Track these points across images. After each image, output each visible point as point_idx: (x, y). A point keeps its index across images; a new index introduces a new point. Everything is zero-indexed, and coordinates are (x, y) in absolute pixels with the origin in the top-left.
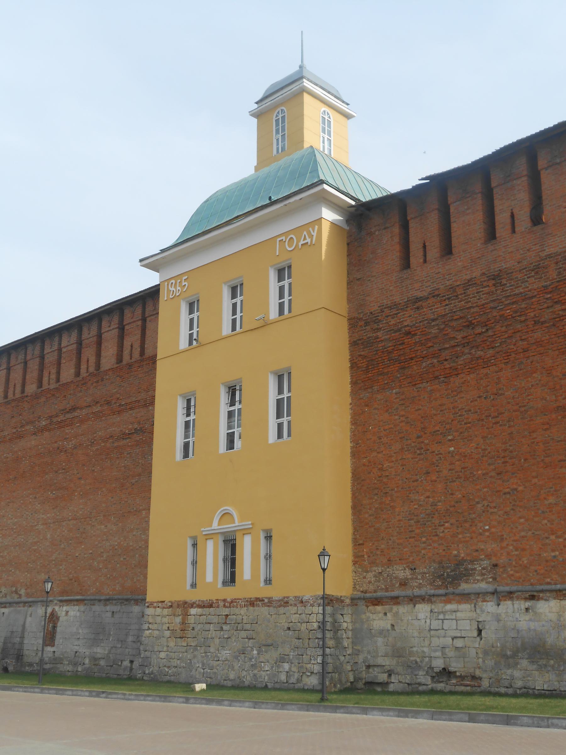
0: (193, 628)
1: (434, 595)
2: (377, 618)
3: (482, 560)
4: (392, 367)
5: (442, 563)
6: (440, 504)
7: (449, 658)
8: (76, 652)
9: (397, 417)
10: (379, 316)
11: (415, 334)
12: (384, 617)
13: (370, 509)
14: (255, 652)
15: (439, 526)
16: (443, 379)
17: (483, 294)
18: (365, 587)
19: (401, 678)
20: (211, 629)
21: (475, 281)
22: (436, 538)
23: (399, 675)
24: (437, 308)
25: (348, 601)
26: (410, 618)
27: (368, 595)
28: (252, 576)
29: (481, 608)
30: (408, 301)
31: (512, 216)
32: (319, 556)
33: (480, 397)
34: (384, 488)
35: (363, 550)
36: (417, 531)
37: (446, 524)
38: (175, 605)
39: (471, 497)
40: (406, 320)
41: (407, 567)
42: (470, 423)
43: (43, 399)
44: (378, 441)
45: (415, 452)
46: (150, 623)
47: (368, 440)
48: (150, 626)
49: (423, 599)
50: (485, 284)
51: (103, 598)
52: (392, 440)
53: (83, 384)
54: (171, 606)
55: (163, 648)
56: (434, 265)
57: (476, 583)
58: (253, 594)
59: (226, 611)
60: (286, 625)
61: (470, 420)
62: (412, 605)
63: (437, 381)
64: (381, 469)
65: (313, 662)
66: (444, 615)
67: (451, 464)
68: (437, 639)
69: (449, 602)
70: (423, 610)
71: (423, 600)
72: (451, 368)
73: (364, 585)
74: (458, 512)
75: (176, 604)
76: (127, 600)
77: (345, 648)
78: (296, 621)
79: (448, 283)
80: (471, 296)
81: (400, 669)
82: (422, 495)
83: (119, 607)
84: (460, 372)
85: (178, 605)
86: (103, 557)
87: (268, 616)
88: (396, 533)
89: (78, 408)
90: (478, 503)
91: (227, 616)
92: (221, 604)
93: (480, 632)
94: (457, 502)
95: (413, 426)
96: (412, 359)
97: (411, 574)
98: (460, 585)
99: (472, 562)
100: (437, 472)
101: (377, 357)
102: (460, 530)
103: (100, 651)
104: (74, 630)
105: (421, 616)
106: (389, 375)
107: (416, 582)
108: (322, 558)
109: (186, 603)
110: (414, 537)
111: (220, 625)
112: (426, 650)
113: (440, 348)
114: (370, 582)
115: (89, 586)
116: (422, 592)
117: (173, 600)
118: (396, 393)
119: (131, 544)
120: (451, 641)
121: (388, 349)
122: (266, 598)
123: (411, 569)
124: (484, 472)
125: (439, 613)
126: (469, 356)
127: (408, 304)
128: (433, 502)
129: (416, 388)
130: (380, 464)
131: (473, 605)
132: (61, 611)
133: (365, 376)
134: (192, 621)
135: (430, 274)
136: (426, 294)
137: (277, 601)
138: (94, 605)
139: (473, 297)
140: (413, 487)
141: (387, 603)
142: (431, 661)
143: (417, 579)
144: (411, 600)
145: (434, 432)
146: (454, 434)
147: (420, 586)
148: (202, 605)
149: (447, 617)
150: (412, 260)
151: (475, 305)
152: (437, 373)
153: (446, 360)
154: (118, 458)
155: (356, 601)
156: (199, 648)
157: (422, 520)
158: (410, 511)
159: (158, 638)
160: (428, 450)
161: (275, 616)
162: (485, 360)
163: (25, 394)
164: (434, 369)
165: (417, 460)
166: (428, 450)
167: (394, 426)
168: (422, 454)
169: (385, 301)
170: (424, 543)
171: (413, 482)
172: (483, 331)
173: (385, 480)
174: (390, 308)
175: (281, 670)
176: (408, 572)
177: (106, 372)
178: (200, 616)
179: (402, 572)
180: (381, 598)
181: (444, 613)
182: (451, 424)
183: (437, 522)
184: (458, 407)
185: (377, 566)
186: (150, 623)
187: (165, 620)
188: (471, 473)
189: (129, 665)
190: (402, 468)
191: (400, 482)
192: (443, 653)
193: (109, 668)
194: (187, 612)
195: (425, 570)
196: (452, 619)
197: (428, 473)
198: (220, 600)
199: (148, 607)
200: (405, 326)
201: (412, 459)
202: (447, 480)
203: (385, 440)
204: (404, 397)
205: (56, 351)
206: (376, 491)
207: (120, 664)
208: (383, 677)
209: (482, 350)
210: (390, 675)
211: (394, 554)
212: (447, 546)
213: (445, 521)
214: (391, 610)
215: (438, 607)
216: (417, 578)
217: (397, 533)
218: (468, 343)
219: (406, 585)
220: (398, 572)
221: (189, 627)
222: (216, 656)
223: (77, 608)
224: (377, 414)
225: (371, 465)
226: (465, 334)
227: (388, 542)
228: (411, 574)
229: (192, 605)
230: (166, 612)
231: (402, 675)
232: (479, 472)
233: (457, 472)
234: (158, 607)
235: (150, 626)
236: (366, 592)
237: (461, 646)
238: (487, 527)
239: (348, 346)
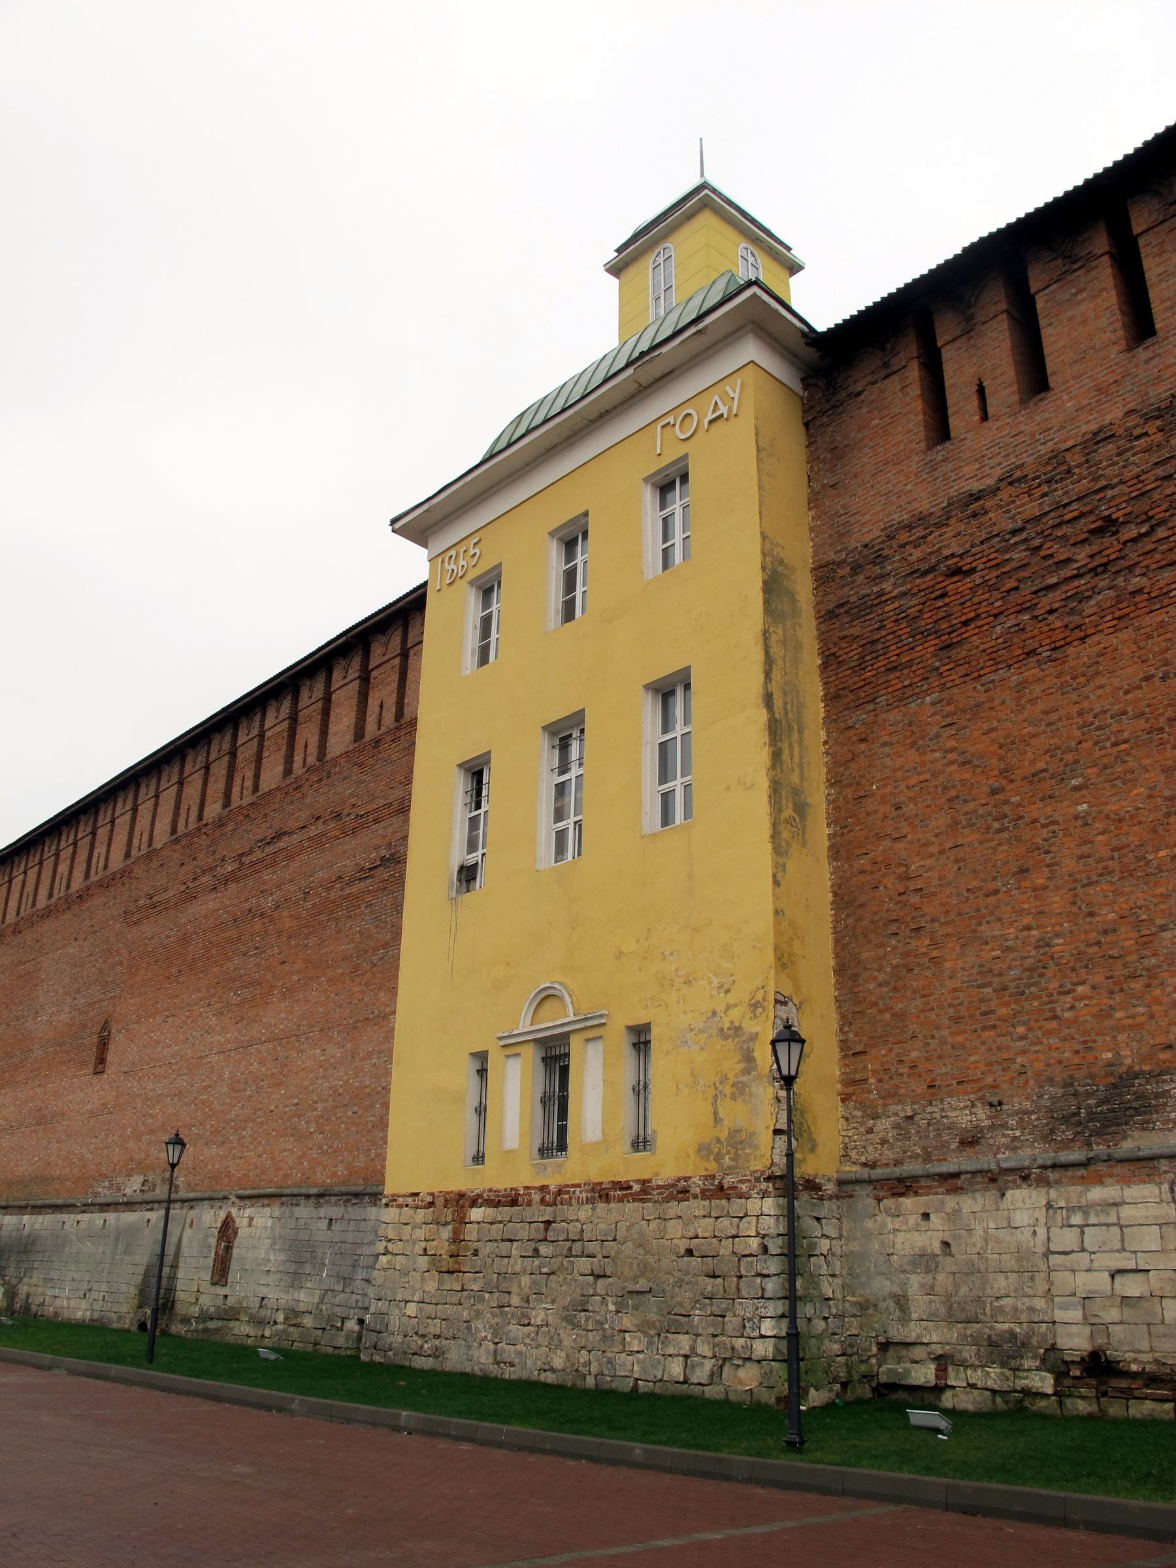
0: (476, 1250)
4: (921, 647)
5: (1071, 1084)
6: (1061, 941)
8: (263, 1298)
9: (937, 754)
11: (973, 570)
13: (879, 971)
15: (1060, 993)
16: (1048, 653)
17: (1134, 455)
18: (871, 1154)
19: (975, 1376)
20: (514, 1252)
21: (1110, 430)
23: (967, 1367)
24: (1023, 505)
25: (830, 1188)
26: (992, 1225)
27: (879, 1172)
30: (949, 505)
32: (167, 1143)
33: (1148, 678)
34: (913, 918)
35: (865, 1068)
36: (1003, 1011)
37: (1080, 989)
38: (440, 1202)
39: (1144, 917)
40: (949, 545)
41: (979, 1099)
42: (1126, 742)
43: (231, 826)
44: (894, 814)
45: (988, 828)
46: (390, 1240)
47: (868, 814)
48: (390, 1246)
49: (1024, 1176)
50: (1138, 431)
51: (313, 1191)
52: (928, 806)
53: (296, 789)
54: (431, 1204)
56: (1007, 420)
59: (547, 1213)
60: (683, 1245)
61: (1125, 735)
63: (1034, 659)
64: (906, 877)
66: (1086, 1214)
67: (1084, 842)
68: (1068, 1274)
69: (1099, 1180)
70: (1024, 1203)
71: (1025, 1178)
72: (1066, 626)
73: (870, 1149)
74: (1111, 957)
75: (442, 1199)
76: (356, 1195)
77: (828, 1299)
78: (707, 1235)
79: (1043, 449)
80: (1104, 463)
81: (968, 1353)
82: (1011, 924)
83: (342, 1210)
84: (1089, 632)
85: (446, 1200)
86: (316, 1109)
88: (946, 1021)
89: (285, 833)
90: (1163, 928)
91: (548, 1223)
92: (536, 1197)
94: (1105, 932)
95: (978, 770)
96: (966, 623)
97: (989, 1118)
100: (1048, 866)
101: (884, 633)
102: (1118, 998)
103: (305, 1298)
104: (262, 1254)
105: (1022, 1218)
106: (913, 668)
109: (461, 1195)
110: (994, 1027)
111: (533, 1244)
112: (1039, 1303)
113: (1035, 588)
114: (884, 1142)
115: (291, 1168)
116: (1023, 1157)
117: (436, 1190)
118: (933, 704)
120: (1108, 1280)
123: (991, 1105)
125: (1071, 1210)
126: (1112, 593)
127: (950, 511)
128: (1043, 939)
129: (983, 685)
130: (900, 865)
132: (242, 1216)
133: (857, 679)
134: (474, 1237)
135: (997, 441)
136: (990, 482)
137: (659, 1187)
138: (298, 1205)
139: (1110, 465)
140: (986, 907)
141: (928, 1191)
143: (1008, 1128)
144: (993, 1180)
145: (1034, 775)
147: (1014, 1145)
148: (494, 1202)
149: (1093, 1220)
150: (953, 422)
151: (1115, 481)
152: (1031, 645)
153: (1051, 612)
154: (350, 917)
155: (849, 1188)
156: (487, 1296)
157: (1014, 984)
158: (981, 966)
159: (404, 1272)
160: (1021, 818)
162: (1153, 595)
163: (204, 822)
164: (1024, 637)
165: (992, 844)
166: (1021, 818)
167: (933, 775)
168: (1007, 829)
169: (894, 516)
170: (1022, 1038)
171: (987, 895)
172: (1143, 530)
173: (914, 899)
174: (910, 527)
176: (982, 1115)
177: (335, 761)
178: (491, 1223)
179: (964, 1114)
180: (915, 1178)
181: (1085, 1210)
182: (1077, 750)
183: (1054, 985)
184: (1091, 710)
185: (900, 1102)
186: (390, 1240)
187: (420, 1233)
188: (1138, 859)
189: (357, 1328)
190: (956, 868)
191: (954, 901)
193: (319, 1332)
194: (464, 1217)
195: (1027, 1105)
196: (1108, 1225)
197: (1023, 871)
198: (534, 1188)
199: (387, 1205)
200: (947, 558)
201: (981, 843)
202: (1075, 881)
203: (909, 809)
204: (952, 708)
205: (358, 681)
206: (893, 928)
207: (339, 1325)
208: (924, 1374)
209: (1143, 575)
210: (942, 1371)
211: (944, 1070)
212: (1085, 1042)
213: (1075, 980)
215: (1066, 1194)
216: (1005, 1126)
217: (950, 1018)
218: (1105, 565)
219: (978, 1143)
220: (955, 1114)
221: (467, 1249)
222: (524, 1315)
223: (267, 1210)
224: (889, 755)
225: (880, 870)
226: (1095, 548)
227: (928, 1044)
228: (989, 1118)
229: (474, 1203)
230: (421, 1215)
232: (1161, 854)
233: (1101, 860)
234: (407, 1206)
235: (390, 1246)
236: (873, 1166)
239: (814, 623)
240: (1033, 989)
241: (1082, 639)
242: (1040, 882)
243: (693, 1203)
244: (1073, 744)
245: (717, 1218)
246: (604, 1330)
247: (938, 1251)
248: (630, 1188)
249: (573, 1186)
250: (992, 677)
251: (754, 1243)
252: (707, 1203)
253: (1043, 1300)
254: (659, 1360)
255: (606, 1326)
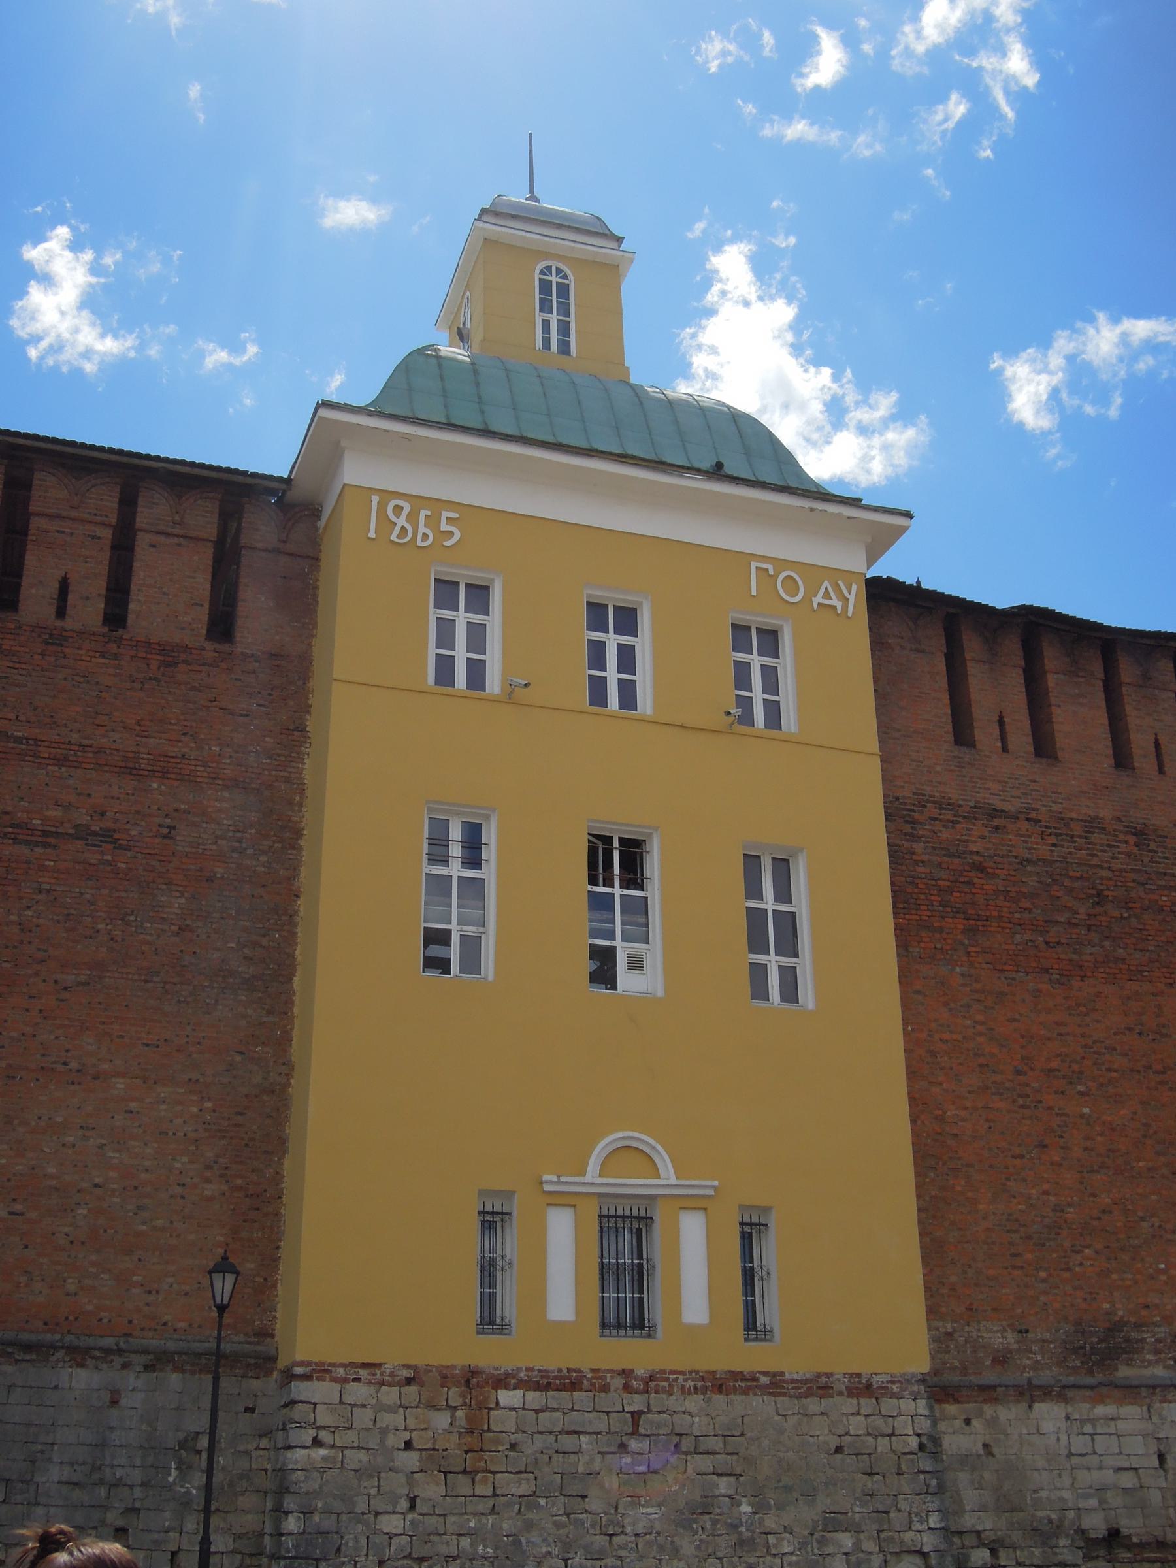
1: (1074, 1386)
2: (950, 1430)
3: (1155, 1324)
7: (1114, 1509)
10: (914, 811)
11: (995, 876)
12: (967, 1428)
14: (746, 1508)
17: (1119, 853)
22: (1067, 1275)
23: (1015, 1549)
26: (1025, 1431)
28: (711, 1317)
29: (1160, 1415)
30: (975, 807)
31: (1157, 744)
32: (210, 1272)
37: (1087, 1251)
45: (1014, 1101)
49: (1046, 1393)
50: (1121, 836)
55: (395, 1504)
57: (1146, 1367)
58: (554, 1361)
59: (637, 1403)
60: (834, 1442)
62: (1025, 1405)
65: (918, 1526)
66: (1094, 1426)
67: (1087, 1138)
68: (1085, 1472)
69: (1101, 1400)
70: (1049, 1415)
79: (1055, 808)
81: (1016, 1536)
87: (777, 1418)
90: (1142, 1219)
92: (618, 1382)
93: (1161, 1457)
94: (1104, 1212)
97: (1018, 1342)
98: (1117, 1370)
99: (1137, 1326)
105: (1048, 1426)
107: (1029, 1358)
108: (217, 1278)
110: (1022, 1267)
112: (1067, 1495)
119: (51, 1170)
121: (939, 882)
122: (765, 1374)
123: (1020, 1332)
124: (1150, 1164)
125: (1083, 1422)
131: (1145, 1408)
137: (793, 1381)
142: (1079, 1517)
143: (1031, 1352)
146: (1090, 1084)
148: (544, 1382)
149: (1099, 1431)
156: (542, 1502)
158: (1010, 1215)
161: (796, 1418)
166: (1040, 1102)
168: (1029, 1107)
170: (1044, 1281)
171: (1014, 1157)
174: (940, 806)
175: (830, 1550)
176: (1011, 1338)
179: (998, 1337)
181: (1093, 1421)
183: (1067, 1244)
192: (1102, 1501)
195: (1048, 1336)
196: (1110, 1434)
200: (971, 852)
204: (978, 986)
210: (994, 1552)
212: (1091, 1293)
214: (980, 1414)
215: (1080, 1410)
221: (498, 1442)
228: (1018, 1342)
229: (502, 1381)
231: (1021, 1548)
232: (1141, 1164)
235: (324, 1435)
237: (1129, 1485)
238: (1162, 1266)
240: (1052, 1243)
241: (1082, 977)
242: (1057, 1159)
243: (837, 1399)
244: (1079, 1058)
245: (866, 1416)
246: (741, 1533)
247: (981, 1452)
248: (757, 1380)
249: (673, 1372)
250: (1013, 975)
251: (914, 1442)
252: (855, 1401)
253: (1070, 1492)
254: (818, 1561)
255: (743, 1529)
